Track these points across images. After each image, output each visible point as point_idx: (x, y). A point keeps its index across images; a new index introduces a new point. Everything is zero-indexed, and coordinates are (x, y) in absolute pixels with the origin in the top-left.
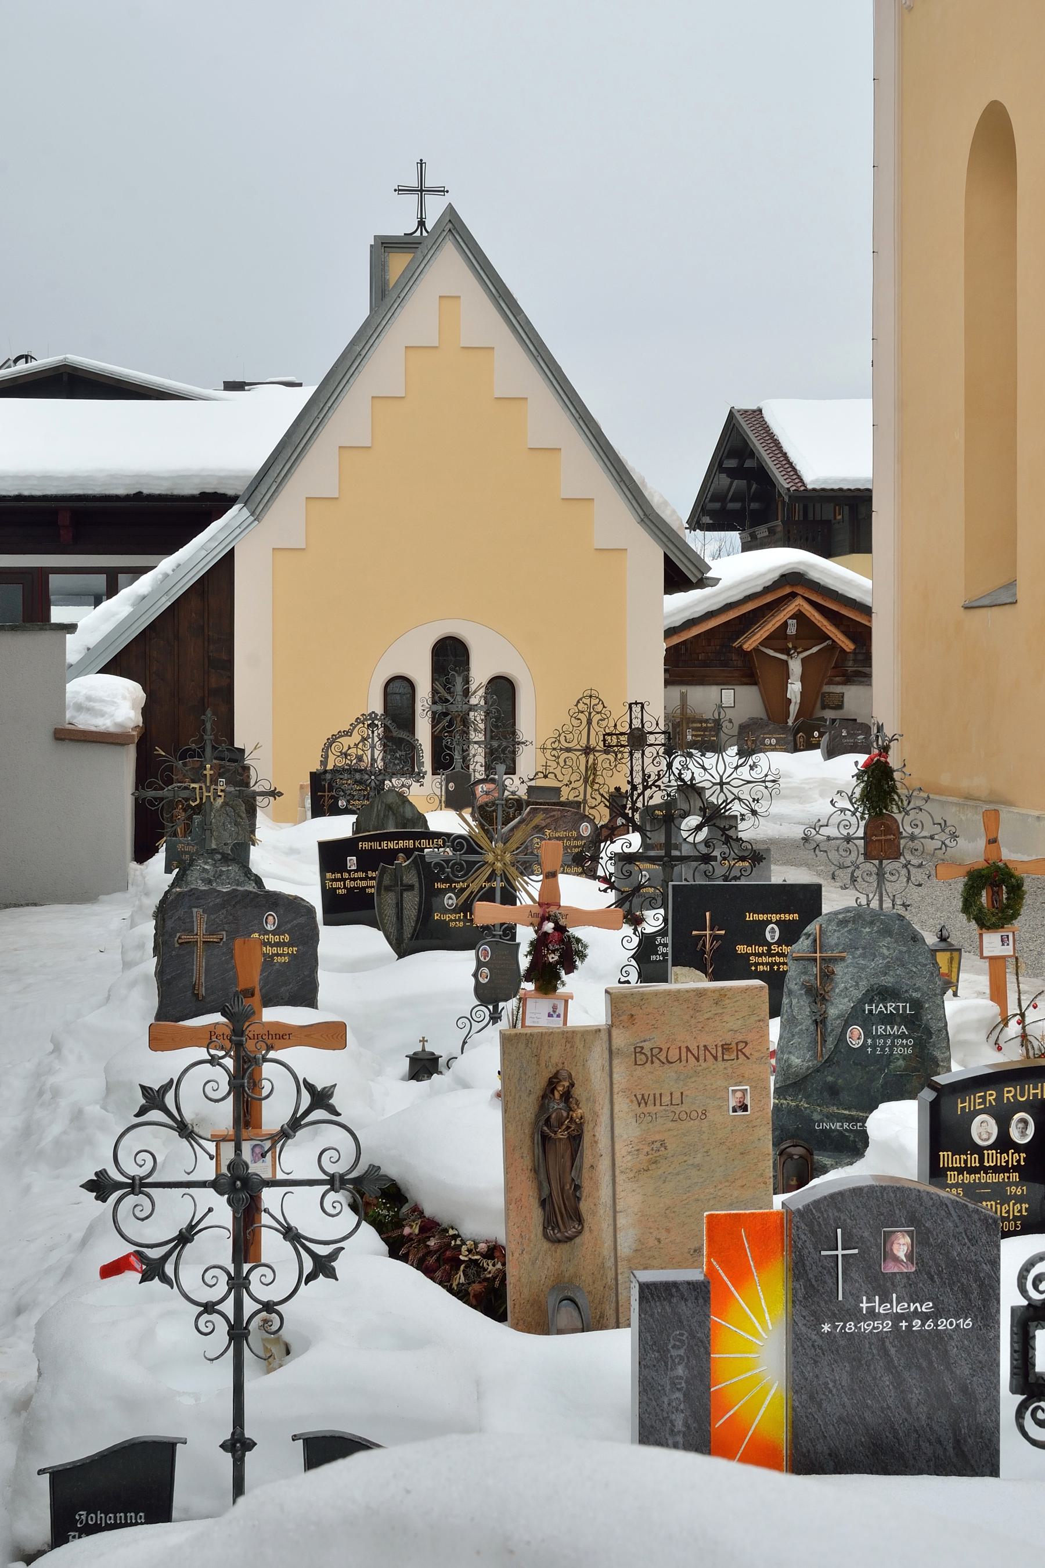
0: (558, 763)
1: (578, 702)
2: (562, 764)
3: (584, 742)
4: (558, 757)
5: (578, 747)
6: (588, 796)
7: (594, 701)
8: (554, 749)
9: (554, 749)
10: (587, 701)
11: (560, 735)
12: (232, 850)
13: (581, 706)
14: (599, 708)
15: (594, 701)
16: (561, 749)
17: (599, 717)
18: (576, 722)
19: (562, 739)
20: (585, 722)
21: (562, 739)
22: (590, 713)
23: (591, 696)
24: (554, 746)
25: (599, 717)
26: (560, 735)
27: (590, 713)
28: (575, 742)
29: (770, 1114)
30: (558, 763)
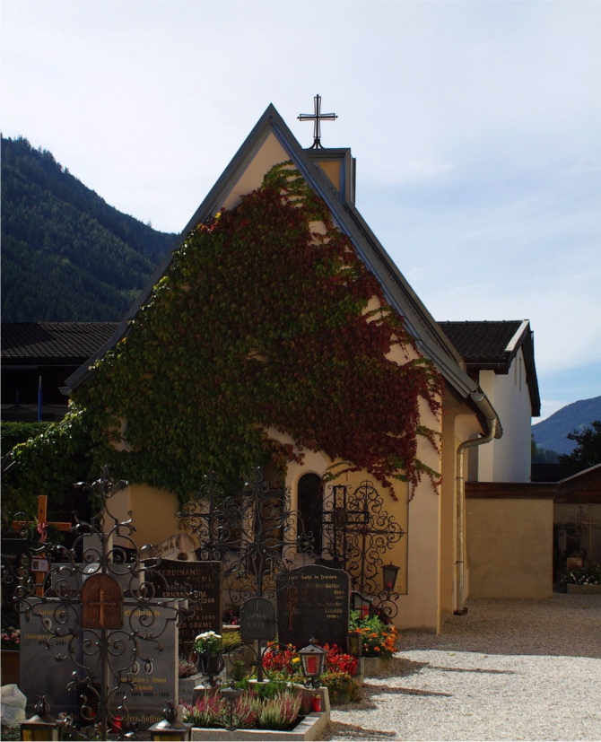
0: (389, 521)
1: (356, 491)
2: (386, 521)
3: (368, 538)
4: (388, 526)
5: (372, 534)
6: (365, 569)
7: (369, 491)
8: (392, 533)
9: (392, 533)
10: (364, 491)
11: (387, 544)
12: (245, 604)
13: (358, 494)
14: (374, 496)
15: (369, 491)
16: (386, 532)
17: (373, 503)
18: (375, 556)
19: (386, 541)
20: (367, 555)
21: (386, 541)
22: (366, 501)
23: (367, 487)
24: (392, 535)
25: (373, 503)
26: (387, 544)
27: (366, 501)
28: (375, 538)
29: (427, 652)
30: (389, 521)
